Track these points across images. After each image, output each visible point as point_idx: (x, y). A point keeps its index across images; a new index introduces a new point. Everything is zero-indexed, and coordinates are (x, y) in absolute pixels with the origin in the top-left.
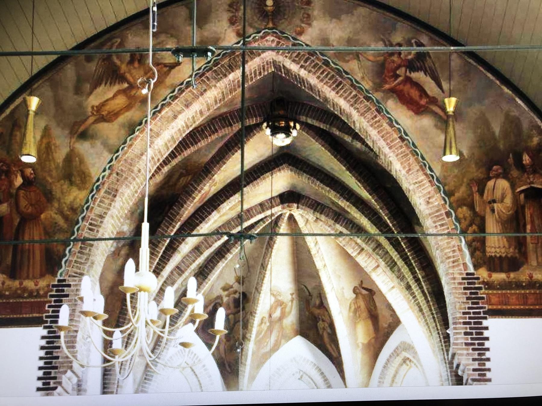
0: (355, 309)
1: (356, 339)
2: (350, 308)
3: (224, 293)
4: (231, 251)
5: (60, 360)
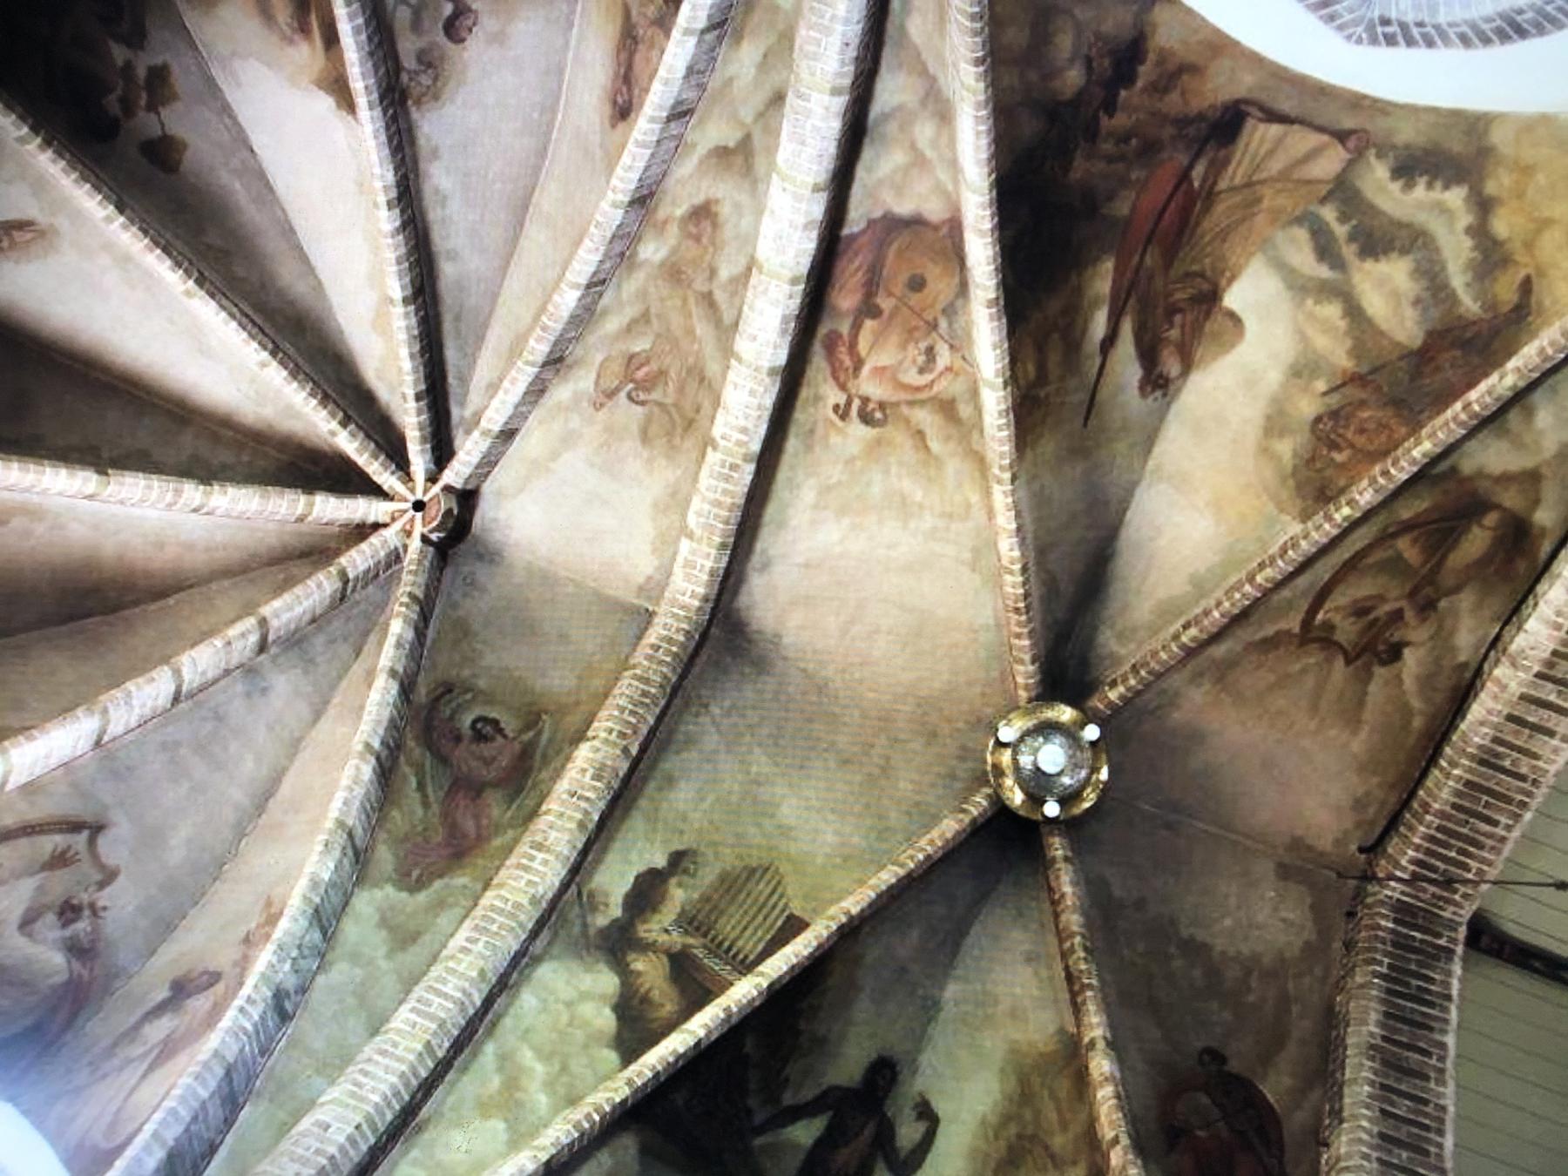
3: (142, 65)
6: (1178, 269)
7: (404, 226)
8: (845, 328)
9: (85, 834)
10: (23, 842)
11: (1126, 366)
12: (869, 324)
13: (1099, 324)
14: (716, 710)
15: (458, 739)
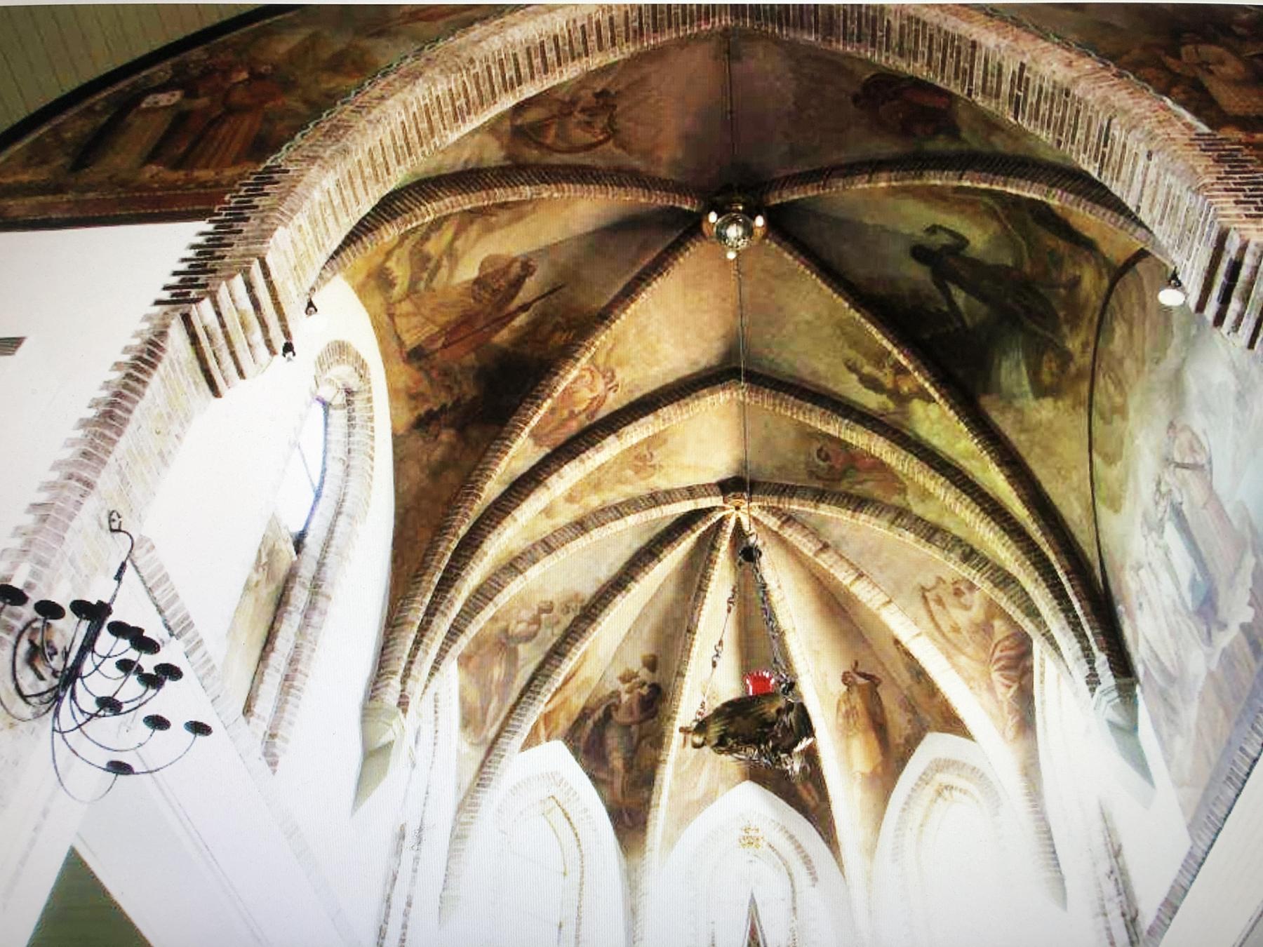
0: (847, 712)
1: (851, 766)
2: (838, 709)
3: (623, 687)
4: (638, 578)
5: (227, 260)
6: (478, 307)
7: (633, 578)
8: (583, 417)
9: (927, 594)
10: (937, 618)
11: (530, 289)
12: (577, 410)
13: (521, 320)
14: (771, 356)
15: (831, 467)
